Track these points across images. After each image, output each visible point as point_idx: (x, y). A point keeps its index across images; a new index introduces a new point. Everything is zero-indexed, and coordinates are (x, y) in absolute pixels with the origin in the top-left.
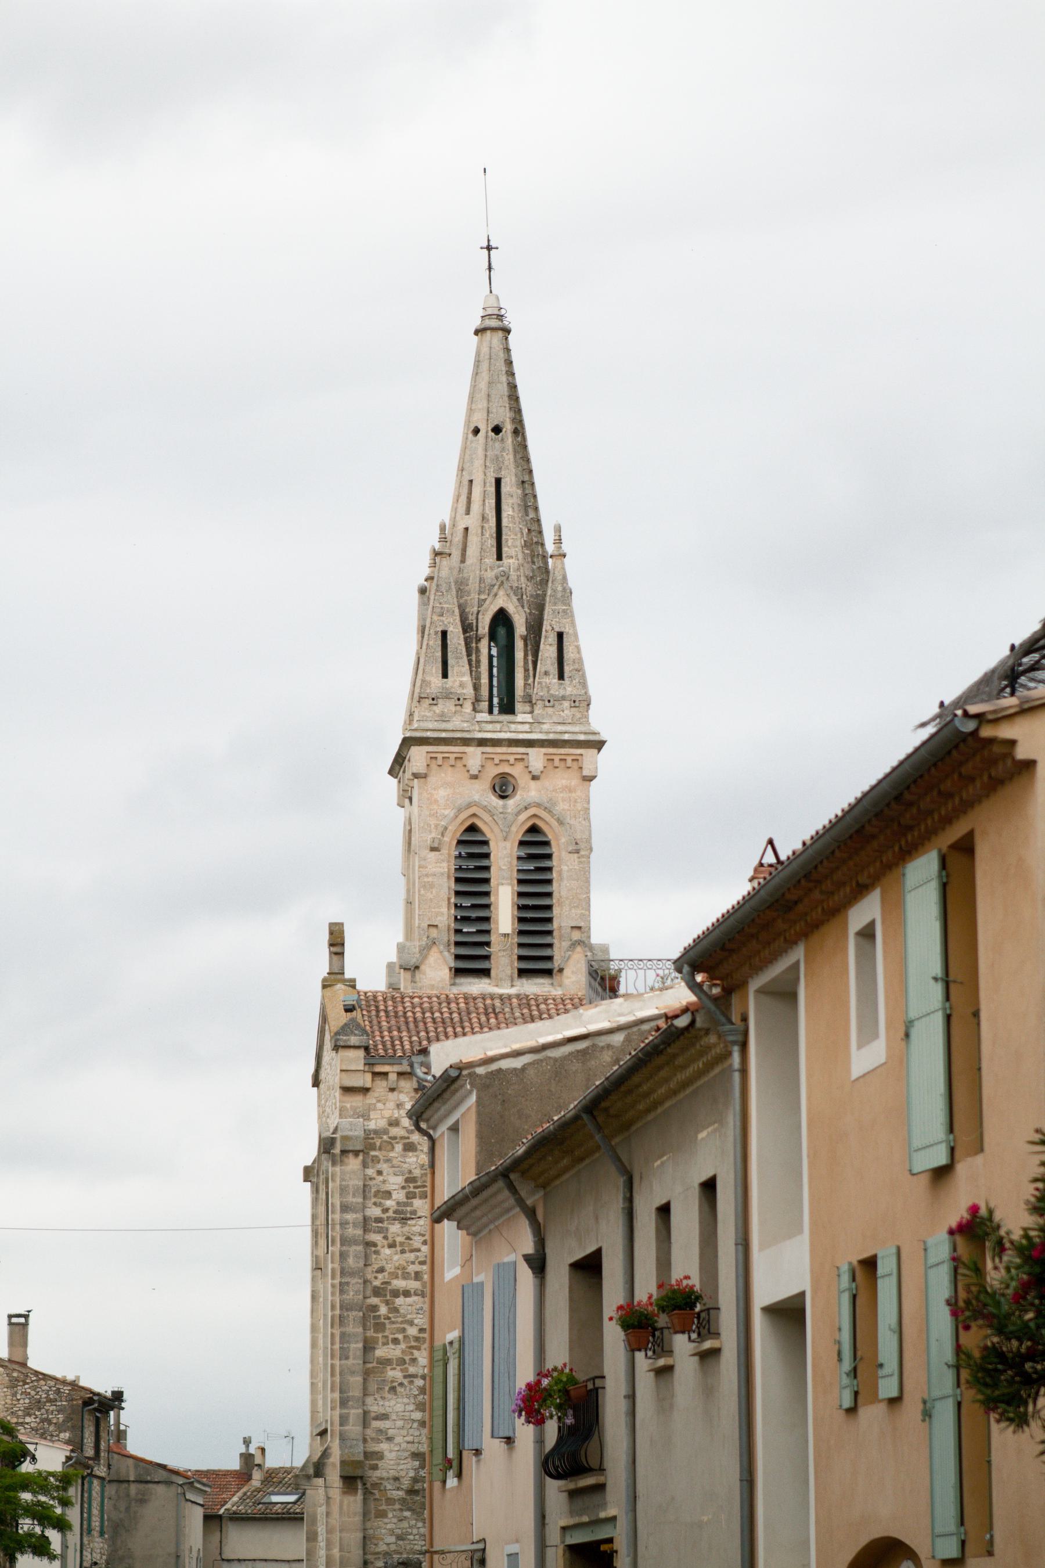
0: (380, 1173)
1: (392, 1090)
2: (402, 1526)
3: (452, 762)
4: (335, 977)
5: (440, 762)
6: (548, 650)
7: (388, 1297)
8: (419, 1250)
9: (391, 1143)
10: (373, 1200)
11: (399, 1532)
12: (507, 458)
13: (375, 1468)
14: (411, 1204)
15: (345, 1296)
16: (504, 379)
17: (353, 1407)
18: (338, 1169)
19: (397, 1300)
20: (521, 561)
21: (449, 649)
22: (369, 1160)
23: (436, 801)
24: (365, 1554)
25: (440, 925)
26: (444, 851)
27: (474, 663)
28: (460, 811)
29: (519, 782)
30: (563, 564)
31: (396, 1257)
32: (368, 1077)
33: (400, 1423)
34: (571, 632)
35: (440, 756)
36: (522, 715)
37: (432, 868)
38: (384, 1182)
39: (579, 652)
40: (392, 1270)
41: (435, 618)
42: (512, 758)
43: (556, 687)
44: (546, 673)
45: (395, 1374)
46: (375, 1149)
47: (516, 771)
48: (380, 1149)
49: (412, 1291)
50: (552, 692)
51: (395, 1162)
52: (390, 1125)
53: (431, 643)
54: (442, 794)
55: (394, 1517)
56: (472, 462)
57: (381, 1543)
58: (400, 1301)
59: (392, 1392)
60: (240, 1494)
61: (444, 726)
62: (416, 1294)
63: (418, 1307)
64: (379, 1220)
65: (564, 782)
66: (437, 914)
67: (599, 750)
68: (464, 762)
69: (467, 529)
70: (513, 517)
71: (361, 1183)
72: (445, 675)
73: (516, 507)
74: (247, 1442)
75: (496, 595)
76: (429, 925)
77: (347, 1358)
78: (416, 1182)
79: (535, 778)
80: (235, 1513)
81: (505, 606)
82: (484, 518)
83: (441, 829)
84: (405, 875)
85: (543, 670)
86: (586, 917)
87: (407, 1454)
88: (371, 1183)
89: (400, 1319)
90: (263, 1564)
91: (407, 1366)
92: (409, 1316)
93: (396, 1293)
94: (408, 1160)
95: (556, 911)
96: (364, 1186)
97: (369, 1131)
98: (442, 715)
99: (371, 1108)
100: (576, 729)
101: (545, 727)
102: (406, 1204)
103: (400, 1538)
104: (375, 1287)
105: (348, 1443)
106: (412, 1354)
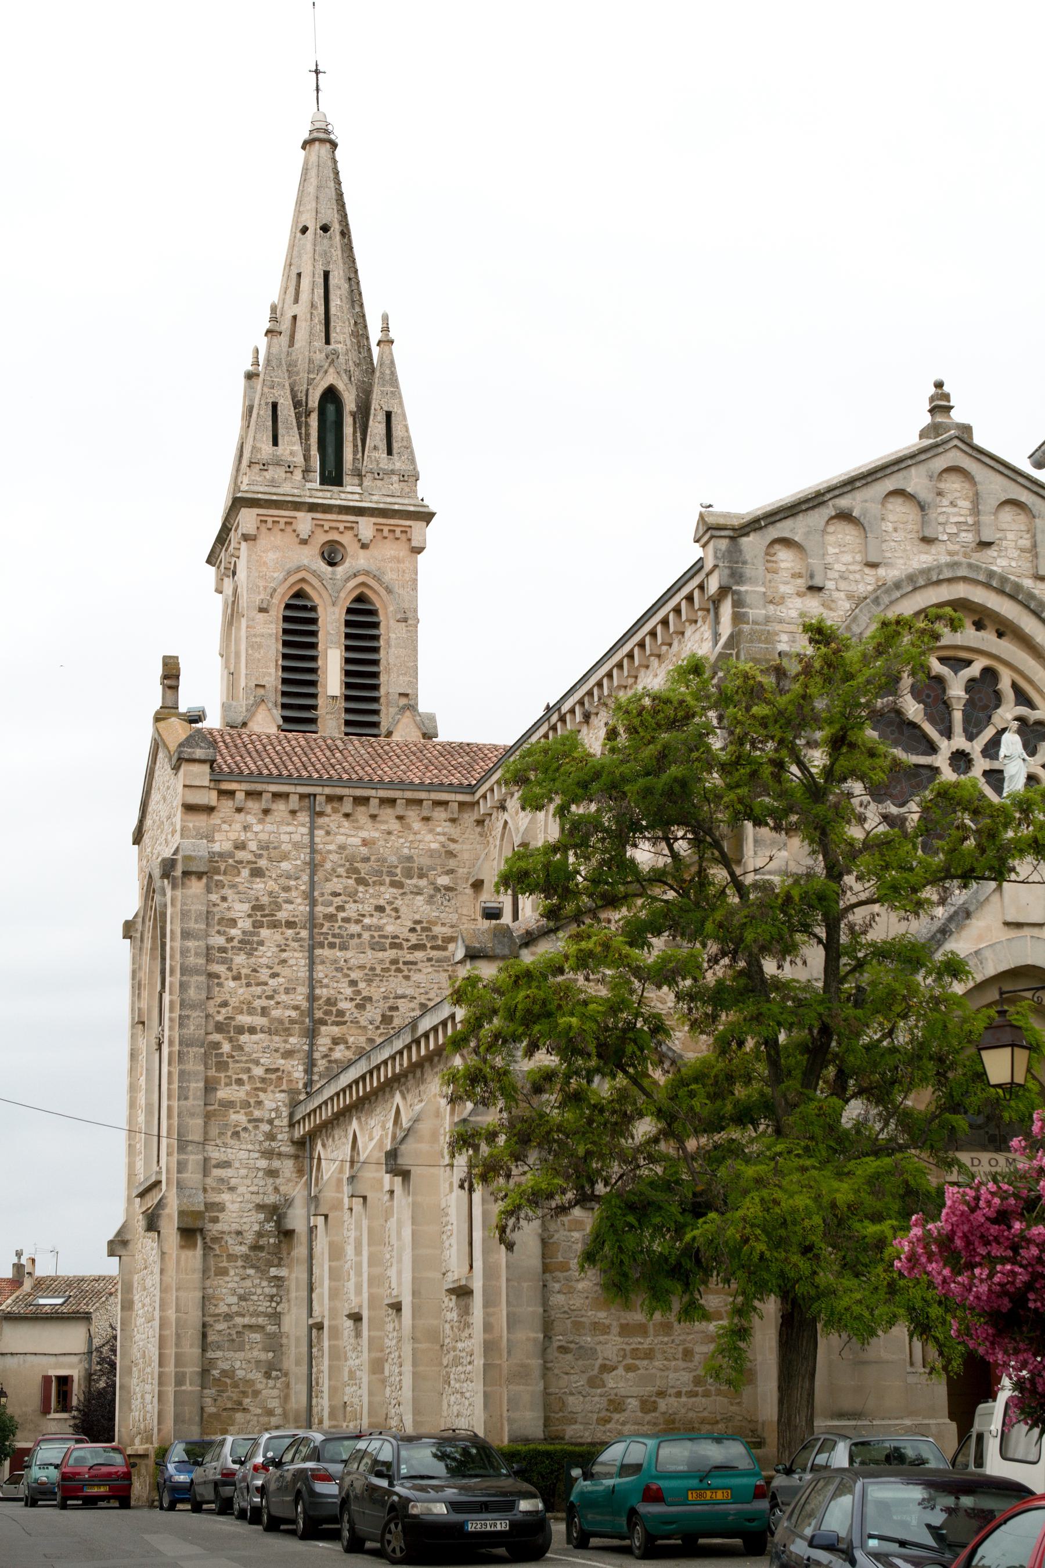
0: (224, 899)
1: (239, 810)
2: (244, 1285)
3: (282, 526)
4: (166, 712)
5: (270, 525)
6: (377, 428)
7: (232, 1034)
8: (266, 984)
9: (236, 867)
10: (217, 928)
11: (241, 1291)
12: (335, 254)
13: (215, 1220)
14: (258, 934)
15: (185, 1031)
16: (332, 184)
17: (192, 1153)
18: (179, 893)
19: (242, 1037)
20: (349, 346)
21: (279, 420)
22: (213, 885)
23: (265, 563)
24: (204, 1316)
25: (267, 686)
26: (273, 612)
27: (303, 436)
28: (289, 574)
29: (349, 549)
30: (391, 350)
31: (241, 991)
32: (214, 794)
33: (243, 1172)
34: (399, 411)
35: (270, 520)
36: (350, 485)
37: (260, 629)
38: (229, 909)
39: (407, 431)
40: (237, 1004)
41: (266, 390)
42: (341, 526)
43: (386, 461)
44: (375, 448)
45: (238, 1118)
46: (219, 874)
47: (346, 539)
48: (225, 873)
49: (258, 1028)
50: (381, 465)
51: (241, 888)
52: (237, 848)
53: (262, 413)
54: (271, 557)
55: (236, 1275)
56: (300, 256)
57: (222, 1304)
58: (244, 1038)
59: (235, 1137)
60: (13, 1297)
61: (274, 490)
62: (262, 1032)
63: (264, 1045)
64: (222, 950)
65: (392, 552)
66: (265, 675)
67: (428, 523)
68: (294, 527)
69: (295, 318)
70: (341, 307)
71: (204, 908)
72: (275, 443)
73: (344, 298)
74: (19, 1254)
75: (326, 372)
76: (257, 685)
77: (186, 1098)
78: (264, 910)
79: (364, 546)
80: (9, 1313)
81: (335, 383)
82: (313, 306)
83: (269, 591)
84: (222, 656)
85: (372, 445)
86: (414, 683)
87: (251, 1206)
88: (215, 909)
89: (244, 1058)
90: (33, 1357)
91: (251, 1109)
92: (255, 1055)
93: (240, 1030)
94: (255, 886)
95: (383, 678)
96: (208, 912)
97: (213, 853)
98: (273, 480)
99: (216, 829)
100: (406, 501)
101: (375, 498)
102: (253, 934)
103: (242, 1298)
104: (218, 1022)
105: (187, 1192)
106: (257, 1096)
